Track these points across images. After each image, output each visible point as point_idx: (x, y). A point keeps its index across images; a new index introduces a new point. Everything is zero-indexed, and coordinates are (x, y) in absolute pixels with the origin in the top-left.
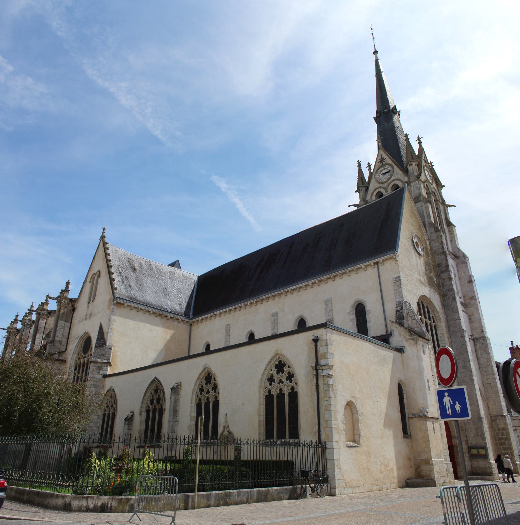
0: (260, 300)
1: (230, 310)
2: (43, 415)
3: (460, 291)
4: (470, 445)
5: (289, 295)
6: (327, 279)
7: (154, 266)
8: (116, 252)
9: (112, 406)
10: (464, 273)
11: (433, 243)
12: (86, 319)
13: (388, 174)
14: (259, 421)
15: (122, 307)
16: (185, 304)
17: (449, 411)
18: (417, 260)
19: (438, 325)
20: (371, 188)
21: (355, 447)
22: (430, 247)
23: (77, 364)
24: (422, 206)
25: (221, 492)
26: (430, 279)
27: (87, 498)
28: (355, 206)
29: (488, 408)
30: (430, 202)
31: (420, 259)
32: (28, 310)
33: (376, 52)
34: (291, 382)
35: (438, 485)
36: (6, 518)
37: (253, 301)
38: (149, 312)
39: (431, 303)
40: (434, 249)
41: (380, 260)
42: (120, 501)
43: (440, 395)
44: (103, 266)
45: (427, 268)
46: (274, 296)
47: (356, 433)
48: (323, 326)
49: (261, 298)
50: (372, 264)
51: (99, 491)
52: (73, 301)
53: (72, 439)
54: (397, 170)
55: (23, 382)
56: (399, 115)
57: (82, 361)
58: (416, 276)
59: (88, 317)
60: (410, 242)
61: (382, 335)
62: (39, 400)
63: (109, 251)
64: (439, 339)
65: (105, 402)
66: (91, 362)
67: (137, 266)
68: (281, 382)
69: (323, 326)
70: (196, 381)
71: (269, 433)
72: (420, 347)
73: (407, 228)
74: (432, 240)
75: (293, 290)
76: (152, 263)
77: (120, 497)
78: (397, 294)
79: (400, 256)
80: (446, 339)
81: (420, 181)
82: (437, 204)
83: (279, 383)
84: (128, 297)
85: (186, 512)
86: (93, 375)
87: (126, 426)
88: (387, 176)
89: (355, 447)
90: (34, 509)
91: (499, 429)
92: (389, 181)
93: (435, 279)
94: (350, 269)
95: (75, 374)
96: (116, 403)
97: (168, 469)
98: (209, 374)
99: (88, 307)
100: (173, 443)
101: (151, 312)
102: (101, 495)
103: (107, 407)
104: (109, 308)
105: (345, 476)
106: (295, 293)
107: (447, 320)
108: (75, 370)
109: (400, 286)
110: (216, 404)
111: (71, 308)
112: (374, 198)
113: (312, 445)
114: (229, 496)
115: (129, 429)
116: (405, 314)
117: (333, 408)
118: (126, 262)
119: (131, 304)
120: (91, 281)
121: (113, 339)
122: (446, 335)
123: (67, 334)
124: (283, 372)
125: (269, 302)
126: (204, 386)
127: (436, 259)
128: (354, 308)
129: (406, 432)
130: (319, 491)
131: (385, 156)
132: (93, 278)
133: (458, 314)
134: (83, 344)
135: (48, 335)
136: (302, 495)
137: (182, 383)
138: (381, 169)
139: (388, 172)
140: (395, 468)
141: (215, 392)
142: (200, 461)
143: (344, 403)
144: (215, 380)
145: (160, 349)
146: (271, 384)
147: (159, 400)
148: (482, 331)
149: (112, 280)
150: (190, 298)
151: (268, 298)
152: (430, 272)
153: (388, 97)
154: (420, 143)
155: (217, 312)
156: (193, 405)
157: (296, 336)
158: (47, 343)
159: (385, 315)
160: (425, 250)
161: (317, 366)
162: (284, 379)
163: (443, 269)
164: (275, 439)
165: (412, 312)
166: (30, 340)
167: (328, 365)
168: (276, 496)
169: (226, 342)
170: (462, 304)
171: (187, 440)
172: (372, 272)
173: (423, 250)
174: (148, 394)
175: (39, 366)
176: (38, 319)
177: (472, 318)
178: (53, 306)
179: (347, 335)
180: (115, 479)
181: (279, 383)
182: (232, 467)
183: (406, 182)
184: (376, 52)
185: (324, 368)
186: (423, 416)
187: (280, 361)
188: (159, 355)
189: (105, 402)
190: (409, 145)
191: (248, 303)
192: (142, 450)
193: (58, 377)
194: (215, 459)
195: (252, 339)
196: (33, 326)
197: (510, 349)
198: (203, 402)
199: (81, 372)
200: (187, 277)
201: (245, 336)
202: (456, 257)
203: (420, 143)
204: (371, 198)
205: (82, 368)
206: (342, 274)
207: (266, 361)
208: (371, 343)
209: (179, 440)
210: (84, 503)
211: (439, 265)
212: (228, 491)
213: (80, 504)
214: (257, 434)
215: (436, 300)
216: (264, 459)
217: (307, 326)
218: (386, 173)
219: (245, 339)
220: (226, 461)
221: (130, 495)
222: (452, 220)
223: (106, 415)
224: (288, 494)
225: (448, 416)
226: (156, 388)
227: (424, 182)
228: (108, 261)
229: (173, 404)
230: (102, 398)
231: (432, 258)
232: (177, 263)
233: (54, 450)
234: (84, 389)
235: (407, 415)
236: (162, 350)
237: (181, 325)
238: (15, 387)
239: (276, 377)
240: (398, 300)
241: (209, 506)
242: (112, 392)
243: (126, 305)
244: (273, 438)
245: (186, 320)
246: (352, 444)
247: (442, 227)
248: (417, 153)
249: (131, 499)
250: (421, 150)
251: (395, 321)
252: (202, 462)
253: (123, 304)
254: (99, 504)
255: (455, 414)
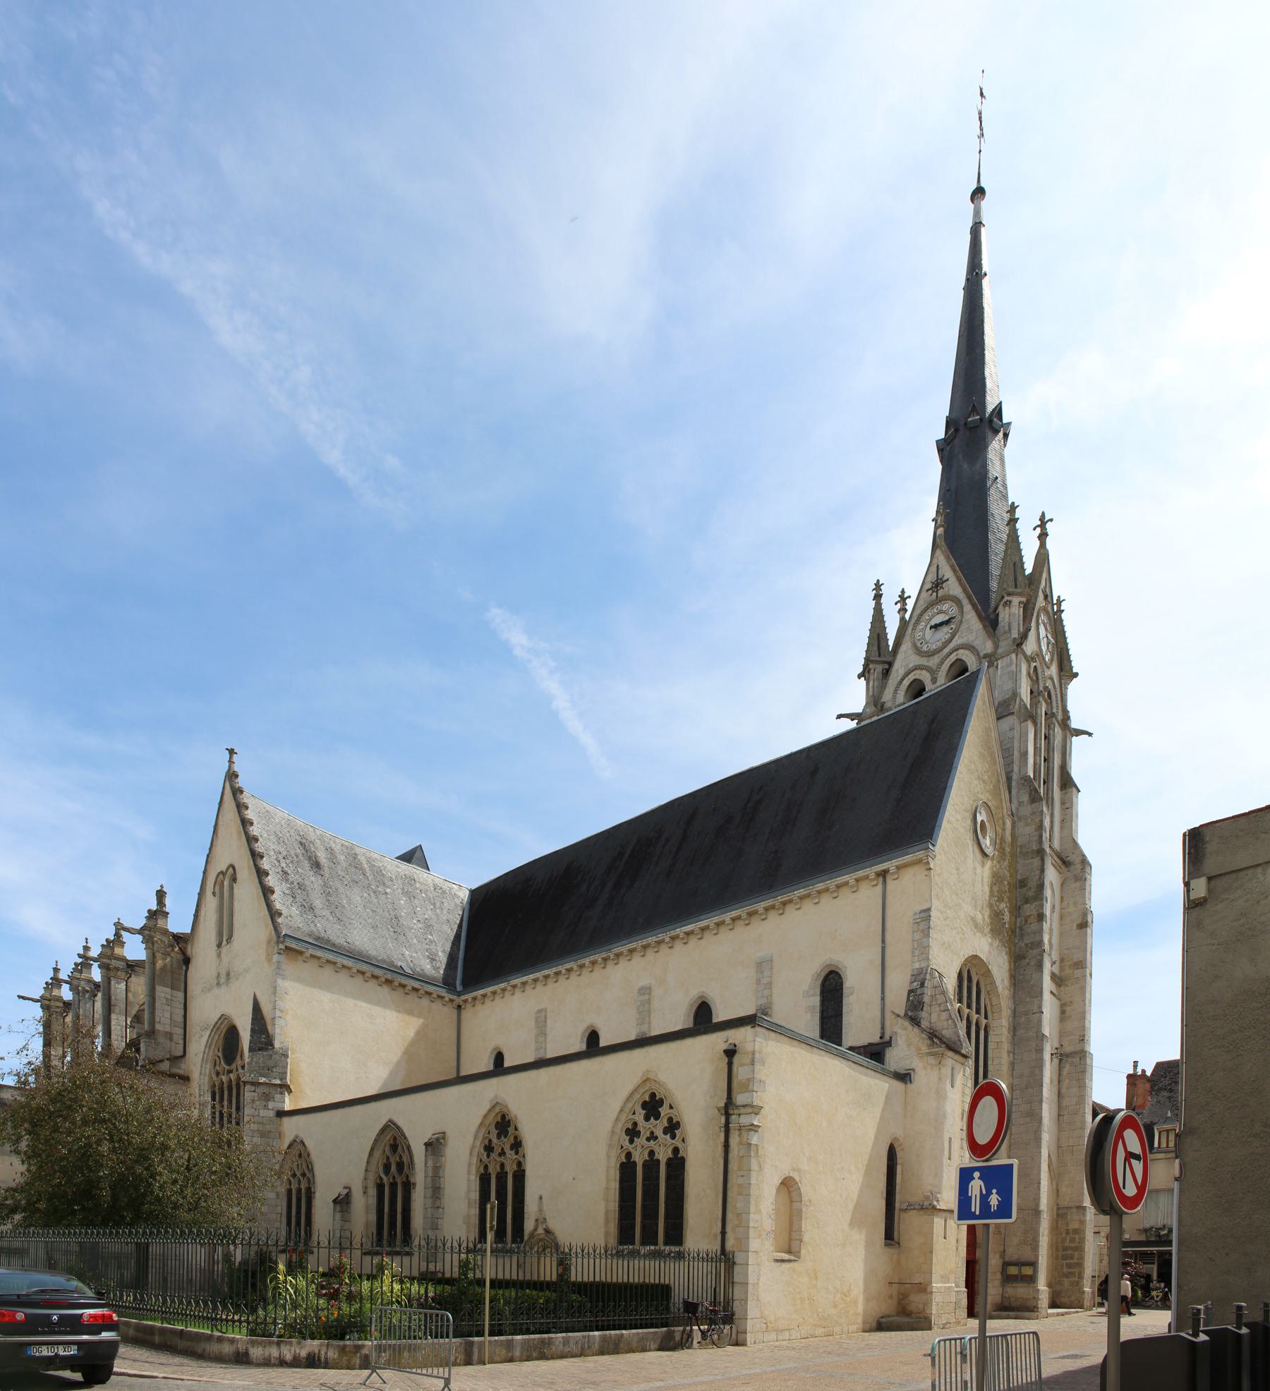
0: (612, 956)
1: (546, 977)
2: (161, 1187)
3: (1055, 947)
4: (1007, 1259)
5: (678, 945)
6: (767, 909)
7: (363, 859)
8: (267, 816)
9: (304, 1175)
10: (1075, 903)
11: (1020, 824)
12: (218, 984)
13: (945, 629)
14: (607, 1212)
15: (300, 958)
16: (442, 958)
17: (976, 1207)
18: (975, 868)
19: (993, 1024)
20: (899, 668)
21: (790, 1261)
22: (1013, 836)
23: (214, 1086)
24: (1012, 729)
25: (532, 1336)
26: (996, 915)
27: (278, 1344)
28: (851, 716)
29: (1056, 1192)
30: (1033, 718)
31: (983, 866)
32: (80, 956)
33: (979, 193)
34: (673, 1137)
35: (935, 1328)
36: (129, 1375)
37: (598, 957)
38: (363, 973)
39: (988, 973)
40: (1020, 841)
41: (890, 865)
42: (343, 1349)
43: (965, 1175)
44: (241, 855)
45: (995, 888)
46: (645, 947)
47: (795, 1236)
48: (749, 1021)
49: (616, 950)
50: (872, 876)
51: (298, 1331)
52: (180, 940)
53: (229, 1237)
54: (971, 618)
55: (104, 1121)
56: (1006, 436)
57: (224, 1078)
58: (967, 908)
59: (222, 980)
60: (969, 822)
61: (870, 1045)
62: (146, 1158)
63: (250, 814)
64: (990, 1068)
65: (287, 1166)
66: (245, 1083)
67: (322, 856)
68: (653, 1137)
69: (749, 1021)
70: (478, 1131)
71: (625, 1234)
72: (946, 1071)
73: (969, 784)
74: (1020, 819)
75: (688, 934)
76: (358, 851)
77: (341, 1343)
78: (917, 952)
79: (938, 857)
80: (1005, 1055)
81: (1020, 656)
82: (1048, 727)
83: (648, 1139)
84: (310, 935)
85: (469, 1369)
86: (254, 1110)
87: (338, 1215)
88: (944, 633)
89: (790, 1261)
90: (177, 1360)
91: (1068, 1232)
92: (946, 650)
93: (1007, 917)
94: (820, 886)
95: (213, 1107)
96: (311, 1170)
97: (431, 1294)
98: (503, 1116)
99: (219, 955)
100: (434, 1249)
101: (369, 975)
102: (304, 1338)
103: (294, 1175)
104: (269, 960)
105: (766, 1313)
106: (693, 941)
107: (1015, 1013)
108: (213, 1099)
109: (926, 933)
110: (520, 1176)
111: (180, 957)
112: (901, 697)
113: (708, 1258)
114: (549, 1344)
115: (346, 1219)
116: (926, 999)
117: (754, 1191)
118: (297, 846)
119: (319, 953)
120: (217, 890)
121: (289, 1032)
122: (1006, 1046)
123: (180, 1019)
124: (657, 1117)
125: (633, 962)
126: (495, 1140)
127: (1019, 867)
128: (819, 982)
129: (889, 1235)
130: (715, 1337)
131: (947, 572)
132: (219, 883)
133: (1041, 1000)
134: (221, 1042)
135: (138, 1018)
136: (684, 1343)
137: (448, 1134)
138: (929, 613)
139: (947, 622)
140: (861, 1300)
141: (517, 1153)
142: (492, 1282)
143: (777, 1181)
144: (516, 1129)
145: (395, 1060)
146: (631, 1141)
147: (400, 1166)
148: (1083, 1039)
149: (267, 892)
150: (453, 944)
151: (631, 951)
152: (1000, 900)
153: (987, 373)
154: (1043, 536)
155: (517, 981)
156: (473, 1177)
157: (689, 1042)
158: (139, 1036)
159: (883, 999)
160: (999, 843)
161: (729, 1108)
162: (659, 1132)
163: (1031, 894)
164: (637, 1247)
165: (944, 993)
166: (99, 1030)
167: (752, 1106)
168: (635, 1345)
169: (537, 1049)
170: (1053, 976)
171: (464, 1245)
172: (868, 895)
173: (994, 843)
174: (378, 1154)
175: (131, 1087)
176: (107, 980)
177: (1068, 1009)
178: (134, 949)
179: (795, 1043)
180: (331, 1312)
181: (648, 1139)
182: (554, 1294)
183: (986, 656)
184: (979, 193)
185: (742, 1110)
186: (928, 1208)
187: (653, 1095)
188: (393, 1073)
189: (287, 1166)
190: (1013, 541)
191: (587, 961)
192: (376, 1260)
193: (181, 1114)
194: (521, 1278)
195: (593, 1046)
196: (100, 995)
197: (1129, 1076)
198: (493, 1170)
199: (226, 1103)
200: (444, 892)
201: (579, 1039)
202: (1064, 862)
203: (1043, 536)
204: (894, 698)
205: (227, 1095)
206: (801, 898)
207: (624, 1094)
208: (845, 1062)
209: (449, 1245)
210: (274, 1352)
211: (1023, 883)
212: (546, 1336)
213: (267, 1354)
214: (602, 1236)
215: (999, 967)
216: (614, 1280)
217: (715, 1020)
218: (941, 624)
219: (579, 1045)
220: (542, 1283)
221: (360, 1339)
222: (1076, 773)
223: (294, 1192)
224: (658, 1342)
225: (974, 1216)
226: (392, 1142)
227: (1030, 659)
228: (251, 840)
229: (430, 1174)
230: (280, 1158)
231: (1010, 865)
232: (417, 854)
233: (196, 1254)
234: (240, 1140)
235: (897, 1205)
236: (398, 1063)
237: (437, 1005)
238: (89, 1131)
239: (643, 1126)
240: (917, 965)
241: (511, 1360)
242: (300, 1147)
243: (308, 954)
244: (633, 1243)
245: (448, 996)
246: (786, 1256)
247: (1049, 790)
248: (1029, 568)
249: (363, 1346)
250: (1042, 558)
251: (902, 1014)
252: (495, 1284)
253: (301, 953)
254: (303, 1353)
255: (986, 1212)
